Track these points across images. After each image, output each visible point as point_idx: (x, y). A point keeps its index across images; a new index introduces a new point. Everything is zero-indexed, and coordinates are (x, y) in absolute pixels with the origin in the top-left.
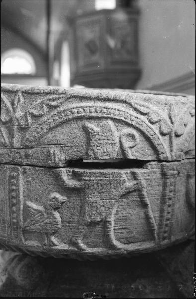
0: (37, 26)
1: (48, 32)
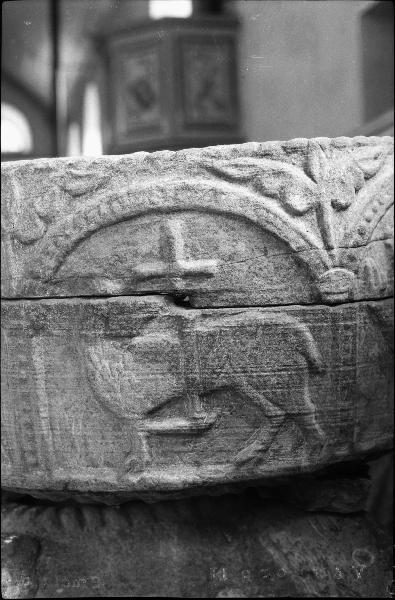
0: (33, 54)
1: (55, 64)
